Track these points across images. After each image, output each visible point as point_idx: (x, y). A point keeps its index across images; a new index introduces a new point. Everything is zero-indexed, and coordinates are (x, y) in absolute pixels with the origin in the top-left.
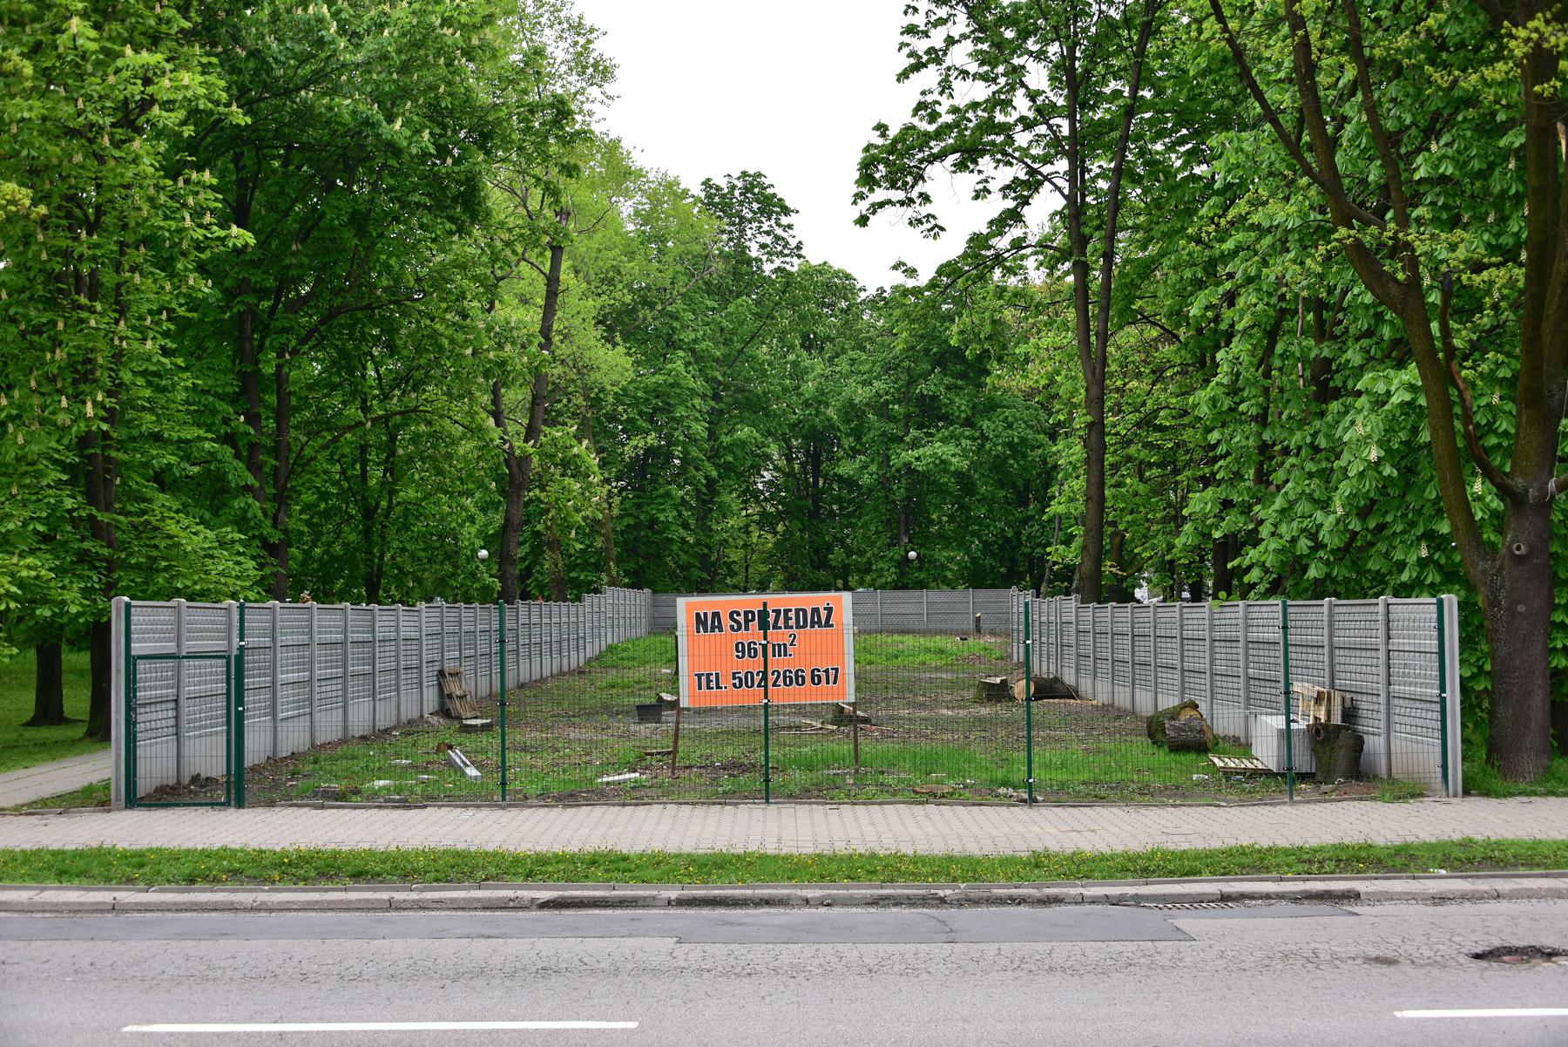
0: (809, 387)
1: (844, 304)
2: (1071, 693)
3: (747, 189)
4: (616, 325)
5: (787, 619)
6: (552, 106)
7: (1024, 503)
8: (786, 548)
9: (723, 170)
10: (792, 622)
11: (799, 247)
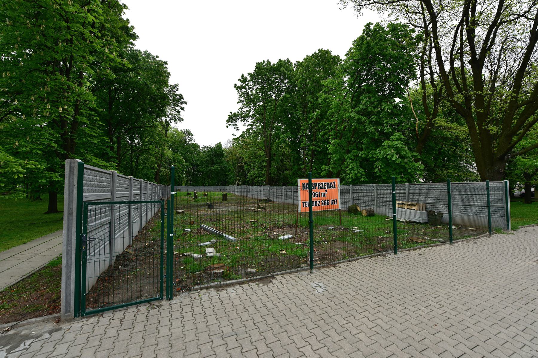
5: (325, 186)
10: (326, 187)
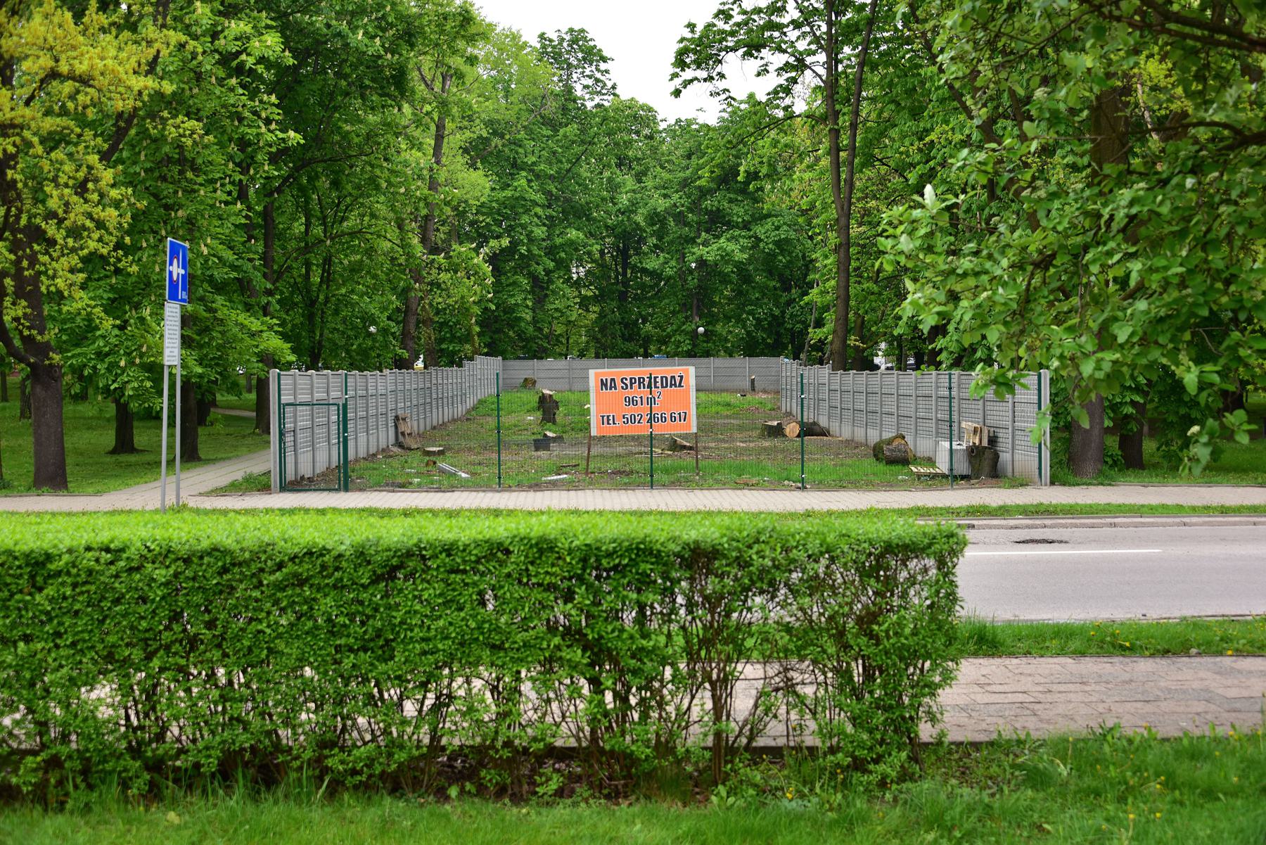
0: (624, 200)
1: (647, 131)
2: (824, 433)
3: (574, 41)
4: (477, 153)
6: (460, 14)
7: (787, 289)
8: (603, 325)
9: (556, 26)
10: (659, 384)
11: (614, 87)
